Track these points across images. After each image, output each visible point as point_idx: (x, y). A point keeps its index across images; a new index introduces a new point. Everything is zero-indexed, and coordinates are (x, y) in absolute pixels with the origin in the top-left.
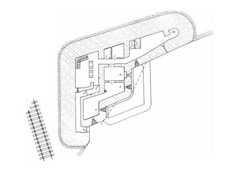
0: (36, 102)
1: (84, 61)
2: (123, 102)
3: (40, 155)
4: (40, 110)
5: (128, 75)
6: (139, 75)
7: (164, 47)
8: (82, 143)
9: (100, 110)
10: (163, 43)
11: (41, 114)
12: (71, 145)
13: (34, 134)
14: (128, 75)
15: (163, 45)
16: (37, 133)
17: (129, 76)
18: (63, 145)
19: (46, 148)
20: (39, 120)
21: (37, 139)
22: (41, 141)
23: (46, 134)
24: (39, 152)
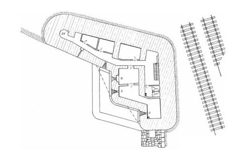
0: (203, 103)
1: (153, 66)
2: (120, 106)
3: (207, 72)
4: (206, 114)
5: (116, 79)
6: (103, 78)
7: (81, 52)
8: (147, 45)
9: (146, 113)
10: (84, 48)
11: (186, 50)
12: (175, 96)
13: (198, 46)
14: (116, 79)
15: (82, 49)
16: (205, 79)
17: (114, 78)
18: (176, 61)
19: (204, 90)
20: (190, 53)
21: (212, 96)
22: (199, 66)
23: (191, 61)
24: (210, 82)
